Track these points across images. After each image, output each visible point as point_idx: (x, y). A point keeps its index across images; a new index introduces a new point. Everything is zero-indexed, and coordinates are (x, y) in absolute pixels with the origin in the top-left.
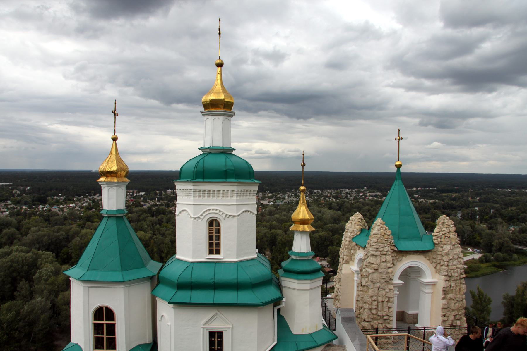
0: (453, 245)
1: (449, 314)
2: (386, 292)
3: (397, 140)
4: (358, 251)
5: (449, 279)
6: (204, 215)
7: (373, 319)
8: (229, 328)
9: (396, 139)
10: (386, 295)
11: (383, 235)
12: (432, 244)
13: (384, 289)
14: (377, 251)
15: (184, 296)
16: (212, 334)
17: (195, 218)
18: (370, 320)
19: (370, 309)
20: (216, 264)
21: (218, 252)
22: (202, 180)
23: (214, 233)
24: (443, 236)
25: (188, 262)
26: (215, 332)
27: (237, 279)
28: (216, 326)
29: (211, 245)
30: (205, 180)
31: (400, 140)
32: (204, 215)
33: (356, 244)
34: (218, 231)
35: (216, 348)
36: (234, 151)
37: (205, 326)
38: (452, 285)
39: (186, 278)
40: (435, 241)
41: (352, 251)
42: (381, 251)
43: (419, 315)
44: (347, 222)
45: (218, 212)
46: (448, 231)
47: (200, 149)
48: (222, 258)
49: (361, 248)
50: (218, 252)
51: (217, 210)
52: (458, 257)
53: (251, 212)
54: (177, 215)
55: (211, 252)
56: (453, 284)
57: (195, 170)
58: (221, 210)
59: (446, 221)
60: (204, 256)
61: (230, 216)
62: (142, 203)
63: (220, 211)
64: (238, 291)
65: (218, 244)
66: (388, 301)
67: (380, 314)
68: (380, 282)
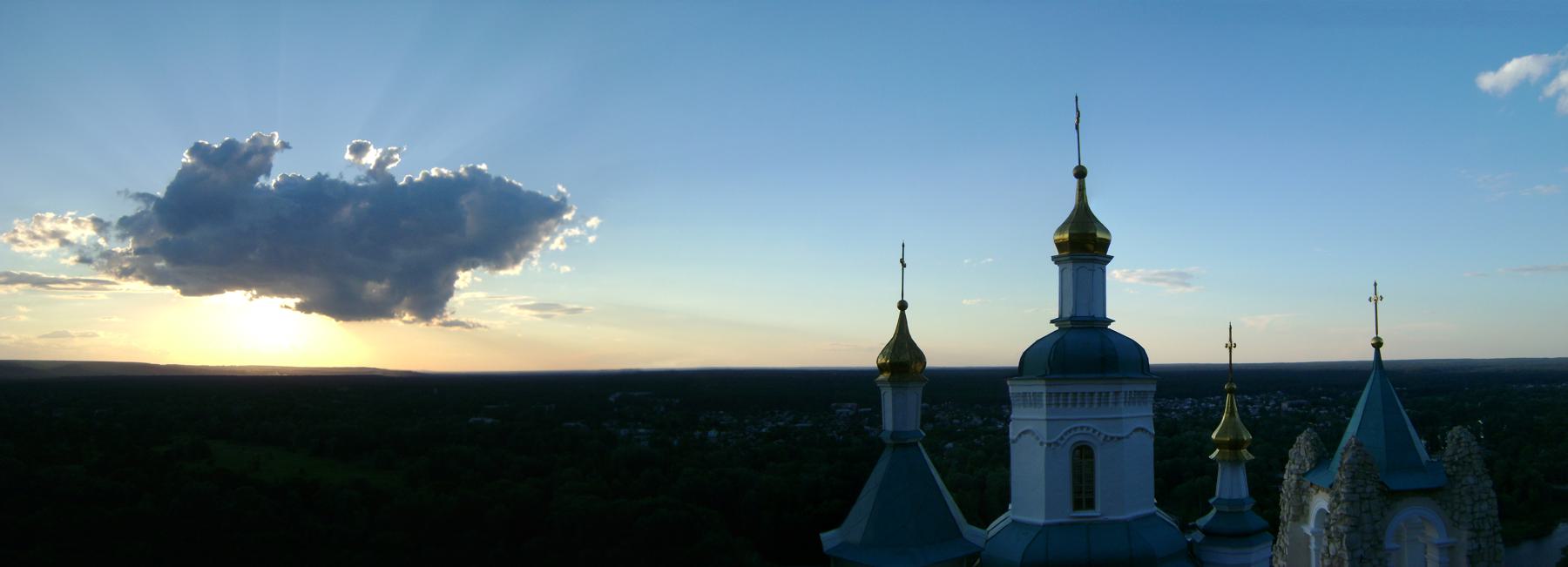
0: (1478, 476)
3: (1373, 302)
4: (1314, 497)
6: (1066, 438)
9: (1370, 300)
11: (1363, 465)
13: (1370, 560)
25: (1036, 526)
29: (1077, 491)
31: (1379, 301)
32: (1066, 438)
33: (1312, 484)
36: (1112, 324)
38: (1483, 546)
40: (1449, 471)
44: (1292, 447)
46: (1467, 452)
47: (1052, 322)
48: (1098, 514)
49: (1320, 492)
50: (1091, 504)
51: (1088, 428)
53: (1147, 431)
54: (1014, 442)
55: (1078, 505)
56: (1483, 544)
58: (1097, 428)
59: (1463, 435)
60: (1067, 514)
61: (1112, 438)
62: (867, 428)
63: (1094, 431)
65: (1091, 491)
68: (1362, 547)
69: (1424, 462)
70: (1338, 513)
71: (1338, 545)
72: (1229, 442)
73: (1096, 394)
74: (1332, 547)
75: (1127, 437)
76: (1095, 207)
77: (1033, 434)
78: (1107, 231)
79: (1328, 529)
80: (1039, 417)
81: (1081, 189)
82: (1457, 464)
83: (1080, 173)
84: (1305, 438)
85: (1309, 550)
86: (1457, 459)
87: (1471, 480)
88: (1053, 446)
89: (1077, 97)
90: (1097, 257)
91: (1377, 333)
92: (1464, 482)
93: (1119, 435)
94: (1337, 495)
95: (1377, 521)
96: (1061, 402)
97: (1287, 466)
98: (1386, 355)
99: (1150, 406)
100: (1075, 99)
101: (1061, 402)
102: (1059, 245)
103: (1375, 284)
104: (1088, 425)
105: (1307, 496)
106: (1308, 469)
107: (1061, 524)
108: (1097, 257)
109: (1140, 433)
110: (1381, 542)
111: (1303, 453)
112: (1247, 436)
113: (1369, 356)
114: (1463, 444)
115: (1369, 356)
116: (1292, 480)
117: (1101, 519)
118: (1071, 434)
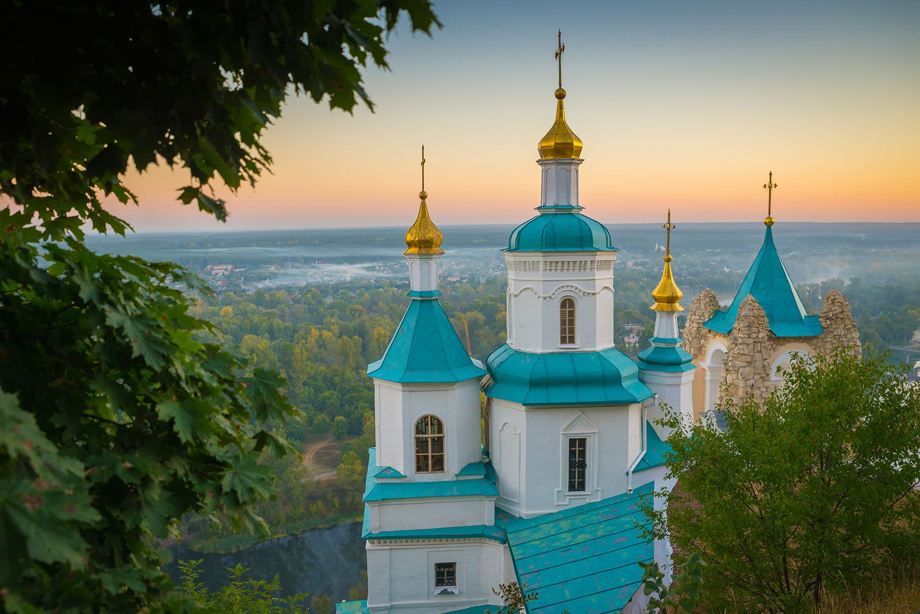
2: (762, 392)
3: (767, 188)
8: (595, 433)
10: (761, 395)
13: (759, 388)
15: (540, 396)
17: (545, 298)
20: (572, 355)
23: (567, 316)
24: (834, 317)
25: (531, 355)
26: (576, 439)
27: (604, 371)
28: (578, 431)
31: (773, 188)
33: (710, 331)
34: (572, 314)
37: (564, 433)
39: (540, 372)
40: (824, 324)
41: (702, 341)
42: (754, 338)
43: (588, 442)
45: (573, 289)
50: (572, 340)
51: (572, 287)
52: (855, 345)
53: (610, 289)
55: (563, 340)
58: (578, 287)
60: (556, 346)
61: (588, 294)
63: (576, 288)
64: (604, 387)
65: (572, 331)
69: (803, 317)
70: (736, 352)
72: (193, 329)
73: (566, 263)
74: (729, 377)
75: (599, 293)
77: (532, 290)
78: (580, 141)
79: (725, 364)
80: (609, 277)
81: (561, 107)
82: (830, 319)
83: (560, 95)
84: (705, 295)
85: (704, 380)
86: (831, 315)
88: (548, 299)
89: (560, 33)
90: (574, 161)
91: (769, 214)
92: (835, 333)
93: (594, 292)
94: (735, 339)
95: (765, 360)
96: (553, 268)
99: (612, 271)
100: (558, 34)
101: (553, 268)
102: (543, 151)
103: (771, 174)
104: (573, 285)
105: (705, 340)
106: (706, 320)
107: (553, 353)
108: (574, 161)
109: (606, 290)
110: (768, 375)
111: (702, 307)
114: (836, 304)
116: (693, 327)
117: (580, 350)
118: (561, 291)
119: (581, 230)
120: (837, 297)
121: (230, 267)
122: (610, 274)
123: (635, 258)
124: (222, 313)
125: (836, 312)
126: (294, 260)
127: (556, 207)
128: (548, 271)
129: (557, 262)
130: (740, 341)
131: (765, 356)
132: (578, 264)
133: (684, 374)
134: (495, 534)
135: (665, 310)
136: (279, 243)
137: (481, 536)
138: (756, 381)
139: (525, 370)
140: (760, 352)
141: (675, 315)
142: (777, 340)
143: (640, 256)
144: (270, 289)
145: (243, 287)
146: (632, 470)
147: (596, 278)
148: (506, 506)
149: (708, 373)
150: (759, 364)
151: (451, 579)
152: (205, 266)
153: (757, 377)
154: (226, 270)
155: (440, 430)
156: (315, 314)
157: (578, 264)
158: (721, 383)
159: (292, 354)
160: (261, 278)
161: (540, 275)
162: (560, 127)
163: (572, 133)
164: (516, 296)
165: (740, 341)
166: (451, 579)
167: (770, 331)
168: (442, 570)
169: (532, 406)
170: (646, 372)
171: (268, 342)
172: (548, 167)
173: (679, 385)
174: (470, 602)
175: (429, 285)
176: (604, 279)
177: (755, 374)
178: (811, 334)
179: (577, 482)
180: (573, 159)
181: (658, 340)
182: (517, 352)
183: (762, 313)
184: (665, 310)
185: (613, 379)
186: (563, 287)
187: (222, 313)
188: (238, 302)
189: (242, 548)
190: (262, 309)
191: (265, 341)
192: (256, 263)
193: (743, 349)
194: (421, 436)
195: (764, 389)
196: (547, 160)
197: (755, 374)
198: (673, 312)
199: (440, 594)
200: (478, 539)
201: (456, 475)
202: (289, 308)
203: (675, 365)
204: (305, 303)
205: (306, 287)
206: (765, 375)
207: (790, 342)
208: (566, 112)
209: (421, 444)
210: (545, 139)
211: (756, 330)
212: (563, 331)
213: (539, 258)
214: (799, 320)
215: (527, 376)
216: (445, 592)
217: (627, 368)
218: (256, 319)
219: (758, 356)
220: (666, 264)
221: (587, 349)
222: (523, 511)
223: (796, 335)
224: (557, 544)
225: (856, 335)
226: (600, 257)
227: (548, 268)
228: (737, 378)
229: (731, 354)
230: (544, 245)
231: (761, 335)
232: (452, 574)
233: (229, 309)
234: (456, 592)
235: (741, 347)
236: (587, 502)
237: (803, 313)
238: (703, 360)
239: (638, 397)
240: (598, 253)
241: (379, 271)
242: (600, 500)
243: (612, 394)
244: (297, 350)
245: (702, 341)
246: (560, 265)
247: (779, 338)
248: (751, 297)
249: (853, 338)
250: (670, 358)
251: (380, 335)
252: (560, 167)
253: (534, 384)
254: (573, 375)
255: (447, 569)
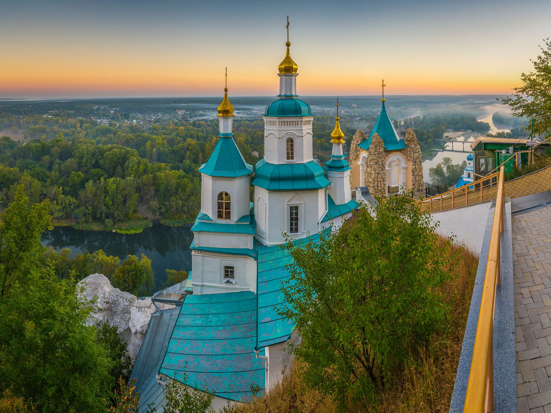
1: (221, 369)
5: (414, 164)
7: (376, 192)
12: (405, 145)
14: (376, 152)
15: (275, 186)
16: (291, 208)
17: (279, 138)
18: (374, 193)
19: (374, 187)
20: (292, 165)
21: (292, 158)
22: (282, 116)
25: (273, 165)
27: (306, 173)
28: (294, 203)
30: (285, 116)
33: (361, 148)
34: (292, 145)
35: (294, 216)
37: (288, 203)
39: (276, 174)
40: (406, 143)
45: (292, 134)
46: (412, 137)
50: (292, 158)
51: (292, 133)
55: (288, 158)
56: (417, 167)
57: (279, 109)
60: (284, 161)
61: (300, 136)
63: (294, 134)
64: (307, 181)
66: (384, 181)
67: (379, 189)
69: (398, 141)
71: (370, 169)
74: (368, 170)
75: (305, 136)
76: (292, 56)
77: (273, 134)
78: (296, 65)
79: (367, 164)
81: (288, 50)
82: (408, 141)
83: (288, 45)
85: (359, 170)
87: (413, 146)
94: (370, 152)
96: (283, 124)
97: (352, 142)
98: (230, 95)
101: (283, 124)
102: (280, 70)
103: (383, 80)
107: (283, 164)
110: (384, 168)
111: (358, 137)
112: (343, 135)
113: (222, 95)
115: (222, 95)
119: (296, 107)
120: (411, 131)
121: (184, 111)
122: (310, 127)
123: (345, 110)
124: (180, 129)
125: (411, 138)
126: (209, 109)
127: (285, 96)
128: (280, 126)
129: (285, 122)
130: (372, 153)
131: (383, 159)
132: (294, 122)
133: (345, 172)
134: (252, 255)
135: (336, 142)
136: (203, 102)
137: (246, 255)
138: (379, 171)
139: (268, 172)
140: (381, 158)
141: (341, 144)
142: (387, 152)
143: (347, 109)
144: (199, 120)
145: (189, 119)
146: (320, 221)
147: (303, 129)
148: (259, 238)
149: (361, 167)
150: (380, 163)
151: (232, 275)
152: (175, 111)
153: (380, 169)
154: (183, 112)
155: (229, 199)
156: (215, 131)
157: (294, 122)
158: (365, 172)
159: (205, 147)
160: (195, 116)
161: (276, 127)
162: (288, 59)
163: (293, 62)
164: (266, 137)
165: (372, 153)
166: (232, 275)
167: (385, 148)
168: (228, 269)
169: (271, 191)
170: (328, 172)
171: (196, 142)
172: (282, 77)
173: (343, 177)
174: (240, 289)
175: (227, 130)
176: (307, 129)
177: (379, 168)
178: (401, 148)
179: (294, 226)
180: (293, 74)
181: (334, 156)
182: (267, 163)
183: (381, 140)
184: (336, 142)
185: (310, 177)
186: (287, 133)
187: (180, 129)
188: (186, 125)
189: (179, 225)
190: (195, 128)
191: (195, 141)
192: (195, 110)
193: (373, 157)
194: (220, 201)
195: (383, 174)
196: (281, 74)
197: (379, 168)
198: (340, 143)
199: (226, 282)
200: (244, 256)
201: (236, 222)
202: (205, 128)
203: (341, 168)
204: (212, 126)
205: (213, 120)
206: (383, 168)
207: (393, 152)
208: (290, 52)
209: (220, 206)
210: (281, 64)
211: (378, 148)
212: (288, 154)
213: (276, 119)
214: (397, 142)
215: (269, 175)
216: (228, 282)
217: (318, 171)
218: (192, 132)
219: (380, 160)
220: (337, 121)
221: (299, 162)
222: (268, 242)
223: (395, 149)
224: (280, 264)
225: (419, 147)
226: (305, 119)
227: (280, 124)
228: (371, 170)
229: (368, 159)
230: (278, 113)
231: (381, 150)
232: (232, 272)
233: (182, 128)
234: (234, 283)
235: (373, 156)
236: (299, 238)
237: (398, 138)
238: (358, 161)
239: (322, 186)
240: (304, 117)
241: (242, 114)
242: (305, 237)
243: (310, 185)
244: (207, 145)
245: (358, 152)
246: (286, 123)
247: (388, 151)
248: (376, 134)
249: (418, 148)
250: (339, 165)
251: (240, 140)
252: (287, 77)
253: (273, 179)
254: (291, 175)
255: (230, 270)
